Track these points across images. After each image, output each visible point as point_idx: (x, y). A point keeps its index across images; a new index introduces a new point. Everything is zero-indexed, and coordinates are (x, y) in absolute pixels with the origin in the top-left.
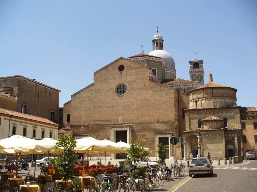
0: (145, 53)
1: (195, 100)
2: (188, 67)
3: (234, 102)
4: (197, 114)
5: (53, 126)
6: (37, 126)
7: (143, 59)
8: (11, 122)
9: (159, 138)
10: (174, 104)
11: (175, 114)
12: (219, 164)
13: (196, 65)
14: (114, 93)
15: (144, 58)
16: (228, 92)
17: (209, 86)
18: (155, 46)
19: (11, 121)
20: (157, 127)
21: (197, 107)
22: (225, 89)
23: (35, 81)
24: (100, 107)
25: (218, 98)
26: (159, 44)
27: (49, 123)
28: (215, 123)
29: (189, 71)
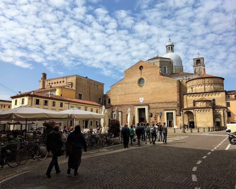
0: (160, 56)
1: (191, 87)
2: (192, 62)
5: (67, 102)
8: (70, 105)
9: (167, 113)
13: (198, 61)
14: (136, 84)
16: (217, 80)
18: (168, 50)
20: (165, 106)
21: (192, 92)
23: (85, 107)
26: (170, 48)
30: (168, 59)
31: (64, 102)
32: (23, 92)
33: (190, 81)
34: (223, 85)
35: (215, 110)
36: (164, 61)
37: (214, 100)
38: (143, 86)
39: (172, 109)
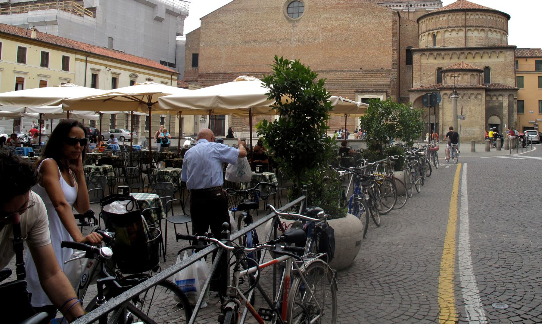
1: (431, 32)
3: (504, 39)
4: (435, 59)
6: (138, 74)
8: (89, 66)
10: (391, 39)
11: (393, 57)
12: (474, 150)
16: (492, 18)
17: (460, 8)
19: (88, 64)
20: (360, 79)
21: (434, 45)
22: (489, 14)
24: (254, 41)
27: (160, 68)
28: (469, 76)
31: (72, 57)
33: (431, 17)
34: (506, 32)
35: (490, 96)
37: (487, 69)
38: (299, 20)
39: (377, 88)
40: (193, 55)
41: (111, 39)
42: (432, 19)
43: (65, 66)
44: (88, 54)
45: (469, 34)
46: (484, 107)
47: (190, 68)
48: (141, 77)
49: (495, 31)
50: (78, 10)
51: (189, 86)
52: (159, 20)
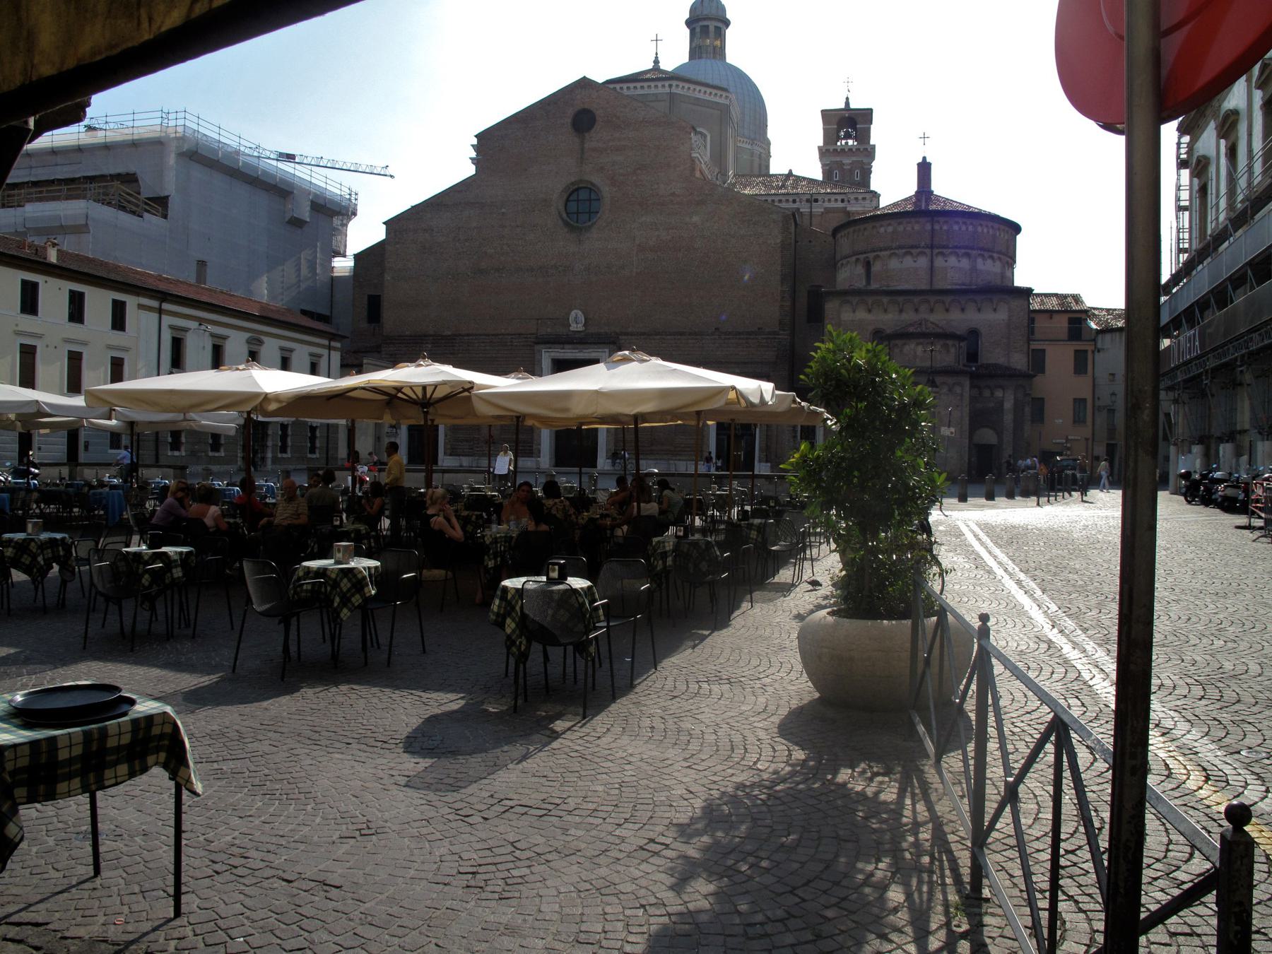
1: (862, 257)
3: (1008, 274)
5: (151, 297)
6: (265, 339)
7: (660, 90)
8: (167, 320)
15: (663, 86)
16: (985, 230)
19: (163, 316)
21: (868, 282)
23: (247, 335)
25: (951, 253)
29: (820, 148)
30: (719, 93)
31: (131, 302)
32: (1176, 140)
33: (862, 227)
36: (698, 101)
40: (370, 297)
41: (202, 264)
42: (865, 229)
43: (119, 322)
44: (163, 296)
45: (939, 262)
46: (967, 410)
47: (364, 325)
48: (236, 343)
49: (991, 257)
50: (129, 202)
51: (365, 361)
52: (297, 223)
